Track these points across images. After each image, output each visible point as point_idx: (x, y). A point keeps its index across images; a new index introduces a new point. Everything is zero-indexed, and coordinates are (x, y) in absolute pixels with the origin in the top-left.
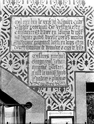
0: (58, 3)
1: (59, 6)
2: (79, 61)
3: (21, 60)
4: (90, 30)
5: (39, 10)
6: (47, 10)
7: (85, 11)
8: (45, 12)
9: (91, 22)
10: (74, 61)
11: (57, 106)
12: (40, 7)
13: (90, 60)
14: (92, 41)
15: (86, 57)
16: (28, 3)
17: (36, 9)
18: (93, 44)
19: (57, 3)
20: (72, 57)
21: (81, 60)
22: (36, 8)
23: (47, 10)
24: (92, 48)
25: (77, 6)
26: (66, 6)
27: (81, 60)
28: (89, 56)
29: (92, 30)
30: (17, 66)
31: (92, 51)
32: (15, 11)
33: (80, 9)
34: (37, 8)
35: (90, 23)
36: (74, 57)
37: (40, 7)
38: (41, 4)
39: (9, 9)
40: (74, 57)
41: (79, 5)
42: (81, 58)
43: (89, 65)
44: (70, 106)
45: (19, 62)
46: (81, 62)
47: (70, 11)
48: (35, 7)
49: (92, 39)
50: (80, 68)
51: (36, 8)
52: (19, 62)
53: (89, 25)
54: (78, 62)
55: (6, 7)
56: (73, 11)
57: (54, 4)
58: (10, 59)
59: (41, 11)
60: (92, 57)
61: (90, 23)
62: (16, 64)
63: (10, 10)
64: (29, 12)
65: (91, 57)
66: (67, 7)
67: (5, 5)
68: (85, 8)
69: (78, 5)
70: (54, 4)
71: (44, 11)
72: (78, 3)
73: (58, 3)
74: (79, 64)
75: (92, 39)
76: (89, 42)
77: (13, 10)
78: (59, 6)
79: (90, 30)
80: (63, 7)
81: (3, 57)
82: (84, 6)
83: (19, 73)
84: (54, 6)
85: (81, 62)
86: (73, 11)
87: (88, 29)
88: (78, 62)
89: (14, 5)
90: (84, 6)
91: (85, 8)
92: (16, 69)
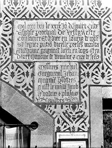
0: (69, 4)
1: (70, 7)
2: (94, 72)
3: (25, 71)
4: (107, 36)
5: (46, 12)
6: (56, 12)
7: (102, 13)
8: (53, 14)
9: (108, 26)
10: (88, 73)
11: (68, 127)
12: (48, 8)
13: (107, 72)
14: (110, 49)
15: (103, 68)
16: (33, 4)
17: (43, 11)
18: (111, 53)
19: (68, 3)
20: (86, 68)
21: (97, 72)
22: (43, 9)
23: (56, 12)
24: (110, 57)
25: (92, 7)
26: (78, 7)
27: (97, 72)
28: (106, 67)
29: (109, 36)
30: (20, 78)
31: (110, 61)
32: (18, 13)
33: (95, 11)
34: (44, 9)
35: (108, 27)
36: (88, 68)
37: (48, 8)
38: (49, 5)
39: (11, 11)
40: (88, 68)
41: (94, 6)
42: (97, 70)
43: (106, 78)
44: (83, 127)
45: (23, 74)
46: (96, 74)
47: (83, 13)
48: (41, 8)
49: (110, 47)
50: (95, 81)
51: (43, 9)
52: (23, 74)
53: (105, 30)
54: (93, 74)
55: (8, 8)
56: (87, 14)
57: (65, 5)
58: (11, 70)
59: (48, 13)
60: (110, 68)
61: (108, 27)
62: (19, 77)
63: (12, 12)
64: (35, 14)
65: (109, 68)
66: (80, 9)
67: (6, 6)
68: (101, 10)
69: (93, 6)
70: (65, 5)
71: (53, 13)
72: (93, 3)
73: (69, 4)
74: (94, 76)
75: (110, 47)
76: (107, 50)
77: (15, 12)
78: (70, 7)
79: (107, 36)
80: (75, 9)
81: (4, 68)
82: (100, 8)
83: (23, 87)
84: (64, 7)
85: (96, 74)
86: (87, 14)
87: (105, 35)
88: (93, 74)
89: (17, 6)
90: (100, 8)
91: (101, 10)
92: (19, 83)
